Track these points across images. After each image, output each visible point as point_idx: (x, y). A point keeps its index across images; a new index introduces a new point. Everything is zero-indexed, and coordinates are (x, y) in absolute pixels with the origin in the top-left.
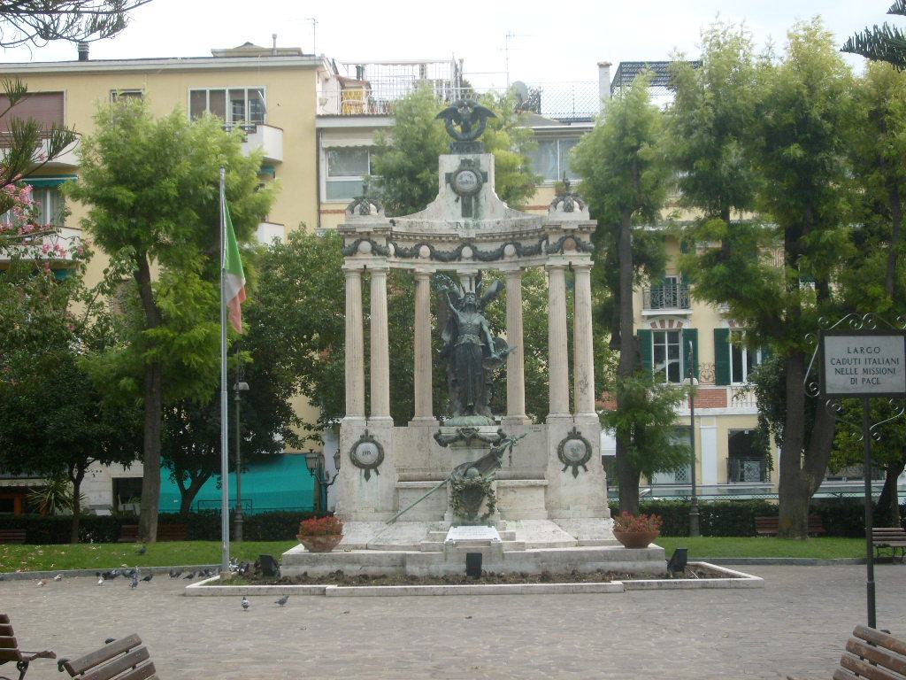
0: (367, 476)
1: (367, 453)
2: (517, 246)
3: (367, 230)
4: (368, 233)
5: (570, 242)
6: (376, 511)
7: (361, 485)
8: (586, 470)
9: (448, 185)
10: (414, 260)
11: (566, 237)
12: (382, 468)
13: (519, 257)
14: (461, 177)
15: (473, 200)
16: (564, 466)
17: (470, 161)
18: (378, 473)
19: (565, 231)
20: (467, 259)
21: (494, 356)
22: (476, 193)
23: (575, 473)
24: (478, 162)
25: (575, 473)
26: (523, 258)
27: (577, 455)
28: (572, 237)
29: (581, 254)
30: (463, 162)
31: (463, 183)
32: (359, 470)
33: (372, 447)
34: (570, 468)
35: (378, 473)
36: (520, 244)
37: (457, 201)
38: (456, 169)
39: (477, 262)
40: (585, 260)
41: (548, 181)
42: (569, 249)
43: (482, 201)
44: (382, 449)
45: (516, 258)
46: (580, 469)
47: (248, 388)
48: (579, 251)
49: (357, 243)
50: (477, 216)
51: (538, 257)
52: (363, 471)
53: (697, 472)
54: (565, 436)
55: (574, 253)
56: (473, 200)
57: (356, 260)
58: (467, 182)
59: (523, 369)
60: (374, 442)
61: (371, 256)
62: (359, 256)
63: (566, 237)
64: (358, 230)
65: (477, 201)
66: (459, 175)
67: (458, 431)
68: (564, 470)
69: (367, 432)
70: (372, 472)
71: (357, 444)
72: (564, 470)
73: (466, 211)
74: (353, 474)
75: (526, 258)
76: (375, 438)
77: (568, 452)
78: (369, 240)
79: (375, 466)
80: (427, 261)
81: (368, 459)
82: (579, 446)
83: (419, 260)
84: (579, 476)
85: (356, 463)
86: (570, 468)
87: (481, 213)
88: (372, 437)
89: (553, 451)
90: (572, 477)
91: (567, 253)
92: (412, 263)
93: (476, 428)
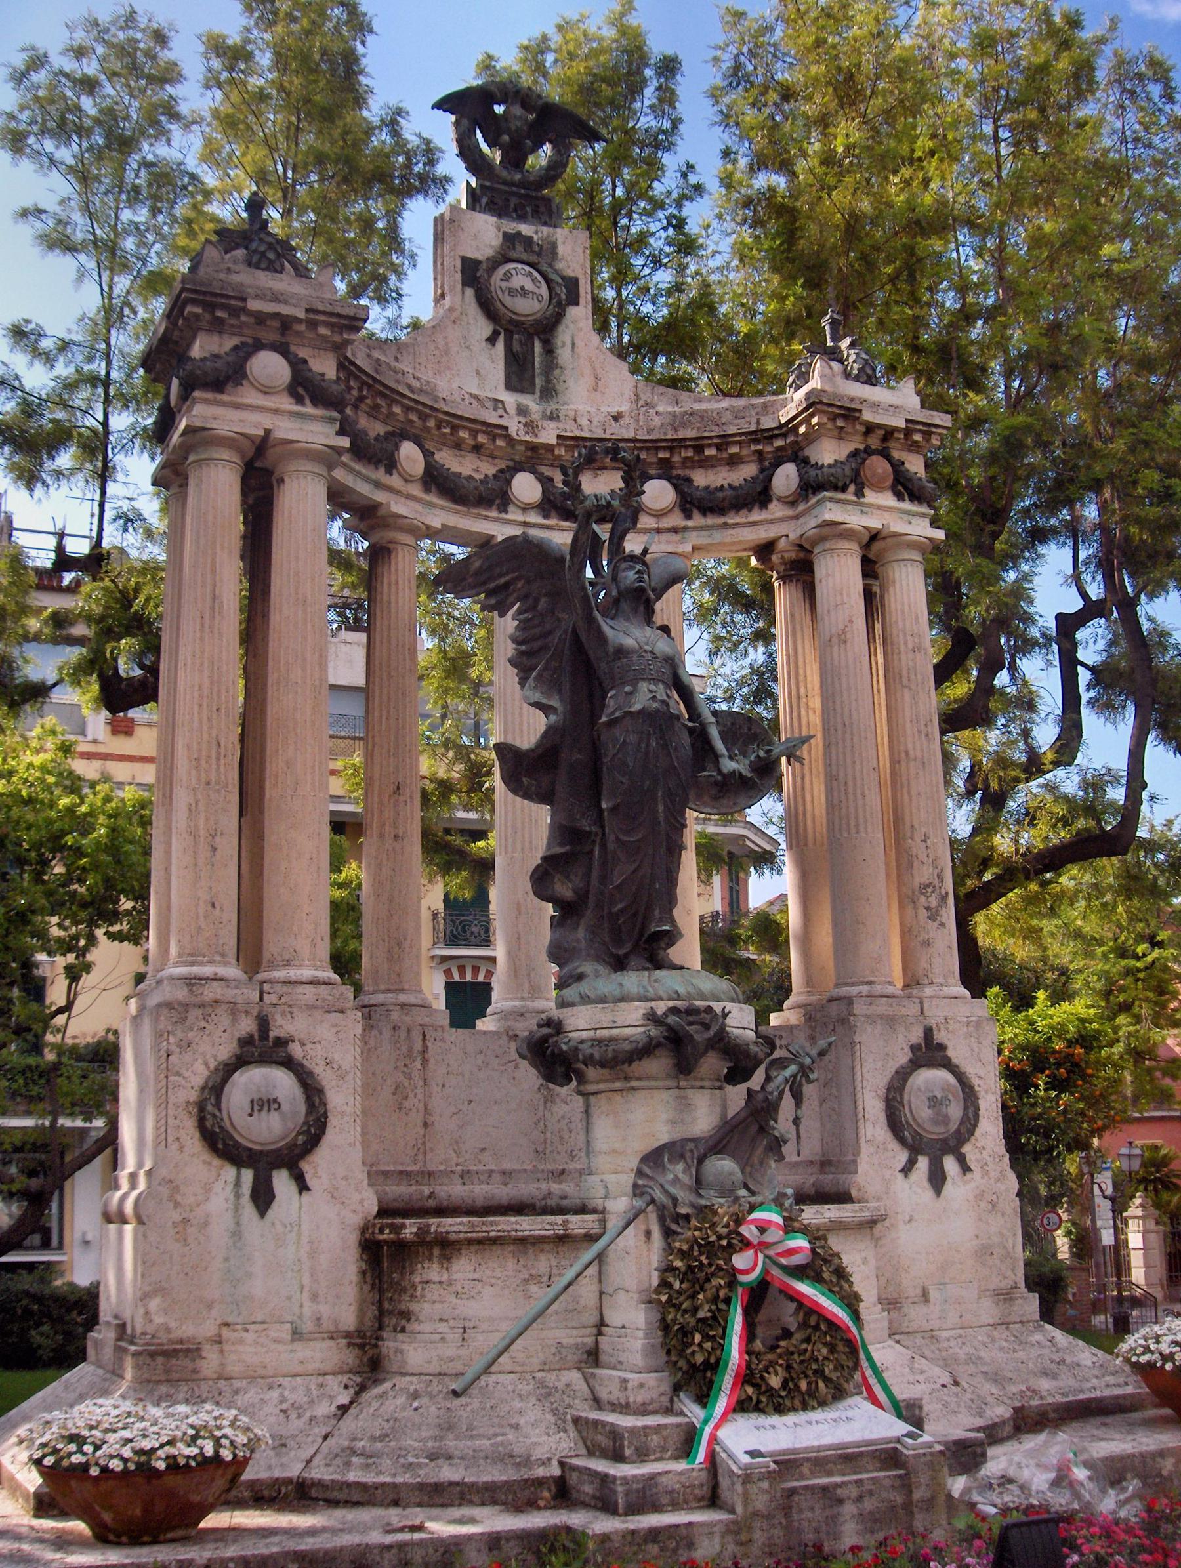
0: (263, 1198)
1: (265, 1104)
2: (681, 485)
3: (285, 310)
4: (286, 323)
5: (878, 466)
6: (297, 1335)
7: (237, 1234)
8: (965, 1168)
9: (470, 292)
10: (380, 474)
11: (868, 451)
12: (318, 1166)
13: (689, 517)
14: (507, 277)
15: (538, 347)
16: (903, 1157)
17: (528, 242)
18: (303, 1187)
19: (870, 428)
20: (526, 508)
21: (728, 765)
22: (546, 329)
23: (937, 1180)
24: (551, 249)
25: (937, 1180)
26: (698, 520)
27: (946, 1120)
28: (885, 454)
29: (907, 505)
30: (510, 239)
31: (512, 292)
32: (230, 1172)
33: (282, 1082)
34: (923, 1163)
35: (303, 1187)
36: (689, 480)
37: (492, 340)
38: (490, 252)
39: (552, 522)
40: (916, 525)
41: (561, 425)
42: (878, 488)
43: (564, 355)
44: (320, 1091)
45: (677, 519)
46: (950, 1165)
47: (163, 557)
48: (899, 497)
49: (245, 352)
50: (549, 393)
51: (756, 515)
52: (248, 1175)
53: (67, 1206)
54: (904, 1058)
55: (888, 499)
56: (538, 347)
57: (238, 406)
58: (523, 292)
59: (492, 907)
60: (289, 1063)
61: (287, 403)
62: (249, 396)
63: (868, 451)
64: (254, 305)
65: (549, 351)
66: (501, 271)
67: (652, 1018)
68: (906, 1170)
69: (264, 1023)
70: (282, 1182)
71: (229, 1069)
72: (906, 1170)
73: (519, 374)
74: (207, 1189)
75: (711, 520)
76: (296, 1050)
77: (918, 1110)
78: (283, 350)
79: (293, 1156)
80: (416, 490)
81: (266, 1131)
82: (946, 1088)
83: (395, 481)
84: (948, 1188)
85: (221, 1143)
86: (923, 1163)
87: (559, 388)
88: (282, 1042)
89: (873, 1107)
90: (929, 1193)
91: (871, 497)
92: (378, 485)
93: (717, 1007)
